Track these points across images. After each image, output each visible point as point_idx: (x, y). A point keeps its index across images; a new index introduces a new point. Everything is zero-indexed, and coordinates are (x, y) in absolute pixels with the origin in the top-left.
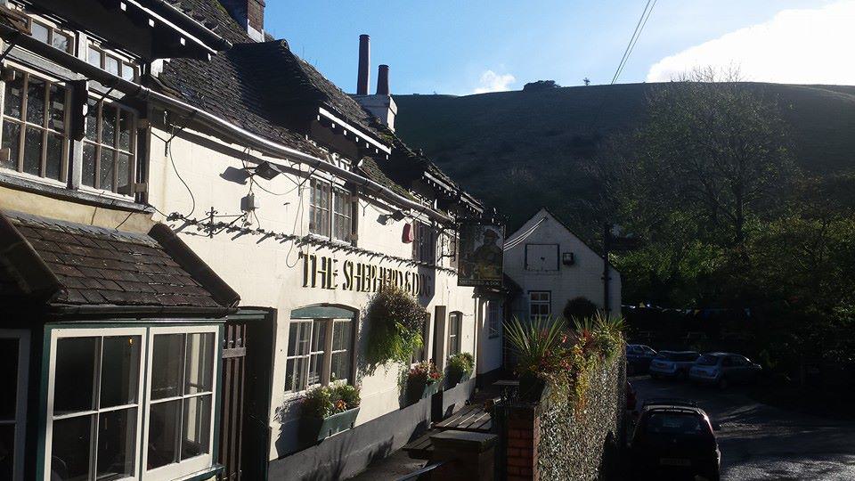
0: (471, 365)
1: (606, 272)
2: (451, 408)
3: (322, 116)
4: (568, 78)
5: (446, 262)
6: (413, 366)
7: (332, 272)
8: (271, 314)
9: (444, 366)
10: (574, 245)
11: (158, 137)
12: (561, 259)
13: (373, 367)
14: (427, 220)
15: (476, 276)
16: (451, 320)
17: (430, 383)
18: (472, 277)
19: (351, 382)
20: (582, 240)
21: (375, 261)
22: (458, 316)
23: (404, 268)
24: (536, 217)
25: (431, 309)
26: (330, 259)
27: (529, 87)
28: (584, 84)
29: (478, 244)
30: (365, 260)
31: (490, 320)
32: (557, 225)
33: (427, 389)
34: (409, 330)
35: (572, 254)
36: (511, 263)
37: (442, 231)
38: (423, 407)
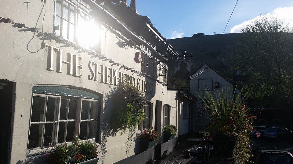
0: (175, 131)
2: (166, 152)
4: (208, 32)
5: (161, 79)
6: (143, 130)
7: (77, 65)
9: (162, 131)
10: (219, 79)
12: (214, 85)
13: (115, 131)
14: (150, 55)
15: (176, 85)
16: (165, 109)
17: (152, 140)
18: (174, 86)
19: (98, 140)
20: (223, 77)
21: (115, 67)
22: (168, 107)
23: (136, 76)
24: (202, 67)
25: (153, 101)
26: (75, 57)
27: (194, 35)
28: (213, 34)
29: (177, 69)
31: (184, 111)
32: (212, 71)
33: (150, 143)
34: (137, 108)
35: (219, 83)
36: (193, 85)
37: (158, 63)
38: (150, 152)
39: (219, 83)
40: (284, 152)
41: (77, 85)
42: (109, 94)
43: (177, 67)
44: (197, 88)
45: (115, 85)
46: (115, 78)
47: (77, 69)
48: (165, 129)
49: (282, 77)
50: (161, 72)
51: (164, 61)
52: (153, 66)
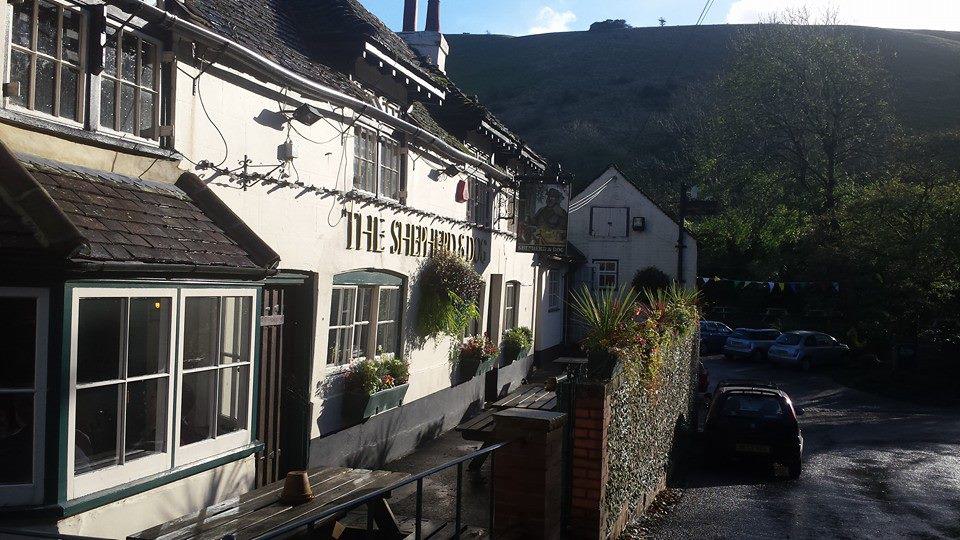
0: (529, 341)
1: (681, 240)
2: (507, 387)
3: (368, 52)
5: (503, 225)
8: (312, 277)
9: (500, 341)
10: (646, 208)
11: (184, 73)
13: (423, 341)
15: (537, 241)
18: (533, 242)
21: (426, 222)
22: (516, 285)
23: (457, 231)
25: (486, 277)
27: (596, 27)
28: (658, 24)
29: (539, 206)
30: (414, 220)
33: (481, 365)
37: (499, 190)
38: (476, 386)
39: (644, 219)
40: (768, 391)
41: (378, 267)
42: (416, 275)
43: (540, 200)
44: (587, 231)
45: (110, 16)
46: (425, 243)
47: (379, 237)
48: (507, 335)
49: (837, 191)
50: (503, 210)
51: (513, 186)
52: (488, 197)
